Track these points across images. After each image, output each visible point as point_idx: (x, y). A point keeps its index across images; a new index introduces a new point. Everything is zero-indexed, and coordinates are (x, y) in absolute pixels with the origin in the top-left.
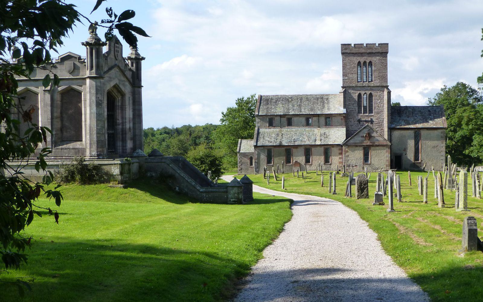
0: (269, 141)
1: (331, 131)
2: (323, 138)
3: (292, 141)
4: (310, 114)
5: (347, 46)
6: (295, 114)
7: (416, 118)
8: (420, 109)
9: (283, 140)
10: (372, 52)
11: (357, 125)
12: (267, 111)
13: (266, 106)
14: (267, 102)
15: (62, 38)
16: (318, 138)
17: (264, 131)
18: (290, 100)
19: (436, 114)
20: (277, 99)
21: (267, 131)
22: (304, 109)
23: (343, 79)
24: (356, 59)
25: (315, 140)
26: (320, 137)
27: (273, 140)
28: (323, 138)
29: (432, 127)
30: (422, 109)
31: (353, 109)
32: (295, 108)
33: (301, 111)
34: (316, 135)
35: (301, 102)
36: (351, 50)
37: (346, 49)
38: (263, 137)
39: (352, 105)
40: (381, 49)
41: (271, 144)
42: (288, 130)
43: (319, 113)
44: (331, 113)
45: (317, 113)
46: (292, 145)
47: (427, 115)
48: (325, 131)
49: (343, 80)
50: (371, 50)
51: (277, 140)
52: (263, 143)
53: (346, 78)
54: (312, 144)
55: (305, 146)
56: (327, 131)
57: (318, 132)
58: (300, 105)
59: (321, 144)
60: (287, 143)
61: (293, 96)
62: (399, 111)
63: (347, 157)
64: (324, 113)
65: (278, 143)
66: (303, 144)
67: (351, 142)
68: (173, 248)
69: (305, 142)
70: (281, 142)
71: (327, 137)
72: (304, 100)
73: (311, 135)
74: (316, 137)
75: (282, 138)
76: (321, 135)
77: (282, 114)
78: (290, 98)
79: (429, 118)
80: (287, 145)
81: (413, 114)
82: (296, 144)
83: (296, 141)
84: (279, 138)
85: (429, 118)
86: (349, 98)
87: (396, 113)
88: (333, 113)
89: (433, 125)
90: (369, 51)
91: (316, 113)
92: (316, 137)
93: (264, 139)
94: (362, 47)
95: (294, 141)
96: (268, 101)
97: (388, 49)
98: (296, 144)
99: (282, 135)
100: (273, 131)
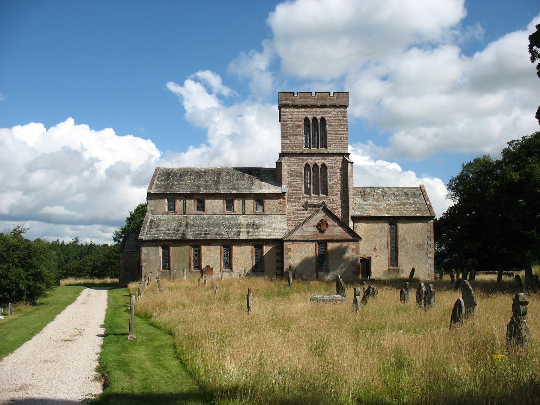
0: (165, 233)
1: (264, 219)
2: (251, 230)
3: (201, 234)
4: (231, 194)
5: (288, 95)
6: (208, 192)
7: (389, 203)
8: (393, 191)
9: (188, 232)
10: (325, 104)
11: (303, 212)
12: (166, 188)
13: (164, 182)
14: (168, 177)
15: (129, 216)
16: (243, 229)
17: (159, 219)
18: (202, 174)
19: (416, 198)
20: (183, 173)
21: (165, 218)
22: (223, 186)
23: (282, 142)
24: (301, 114)
25: (239, 233)
26: (247, 228)
27: (171, 232)
28: (251, 230)
29: (415, 215)
30: (395, 191)
31: (297, 187)
32: (209, 185)
33: (217, 189)
34: (239, 225)
35: (218, 177)
36: (294, 101)
37: (286, 99)
38: (157, 227)
39: (295, 181)
40: (338, 101)
41: (167, 238)
42: (196, 217)
43: (245, 191)
44: (264, 192)
45: (243, 192)
46: (201, 239)
47: (405, 199)
48: (254, 220)
49: (281, 144)
50: (323, 101)
51: (177, 231)
52: (156, 235)
53: (287, 141)
54: (234, 238)
55: (222, 241)
56: (257, 219)
57: (245, 221)
58: (216, 181)
59: (249, 238)
60: (193, 236)
61: (208, 169)
62: (363, 193)
63: (171, 351)
64: (253, 192)
65: (179, 237)
66: (219, 238)
67: (297, 234)
68: (336, 243)
69: (222, 235)
70: (184, 235)
71: (257, 229)
72: (222, 175)
73: (233, 225)
74: (241, 228)
75: (187, 229)
76: (248, 225)
77: (189, 192)
78: (203, 172)
79: (408, 203)
80: (194, 239)
81: (384, 197)
82: (208, 237)
83: (208, 234)
84: (182, 229)
85: (408, 203)
86: (292, 171)
87: (360, 196)
88: (267, 192)
89: (415, 213)
90: (320, 103)
91: (240, 192)
92: (241, 228)
93: (157, 230)
94: (310, 97)
95: (205, 234)
96: (170, 176)
97: (348, 101)
98: (208, 239)
99: (187, 225)
100: (174, 218)
